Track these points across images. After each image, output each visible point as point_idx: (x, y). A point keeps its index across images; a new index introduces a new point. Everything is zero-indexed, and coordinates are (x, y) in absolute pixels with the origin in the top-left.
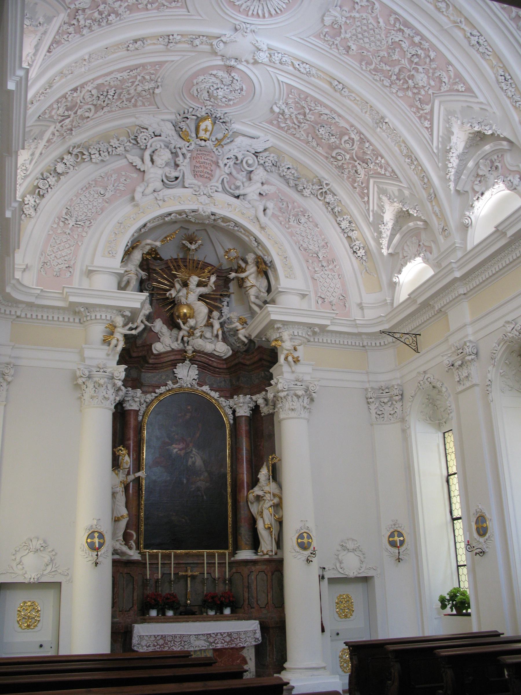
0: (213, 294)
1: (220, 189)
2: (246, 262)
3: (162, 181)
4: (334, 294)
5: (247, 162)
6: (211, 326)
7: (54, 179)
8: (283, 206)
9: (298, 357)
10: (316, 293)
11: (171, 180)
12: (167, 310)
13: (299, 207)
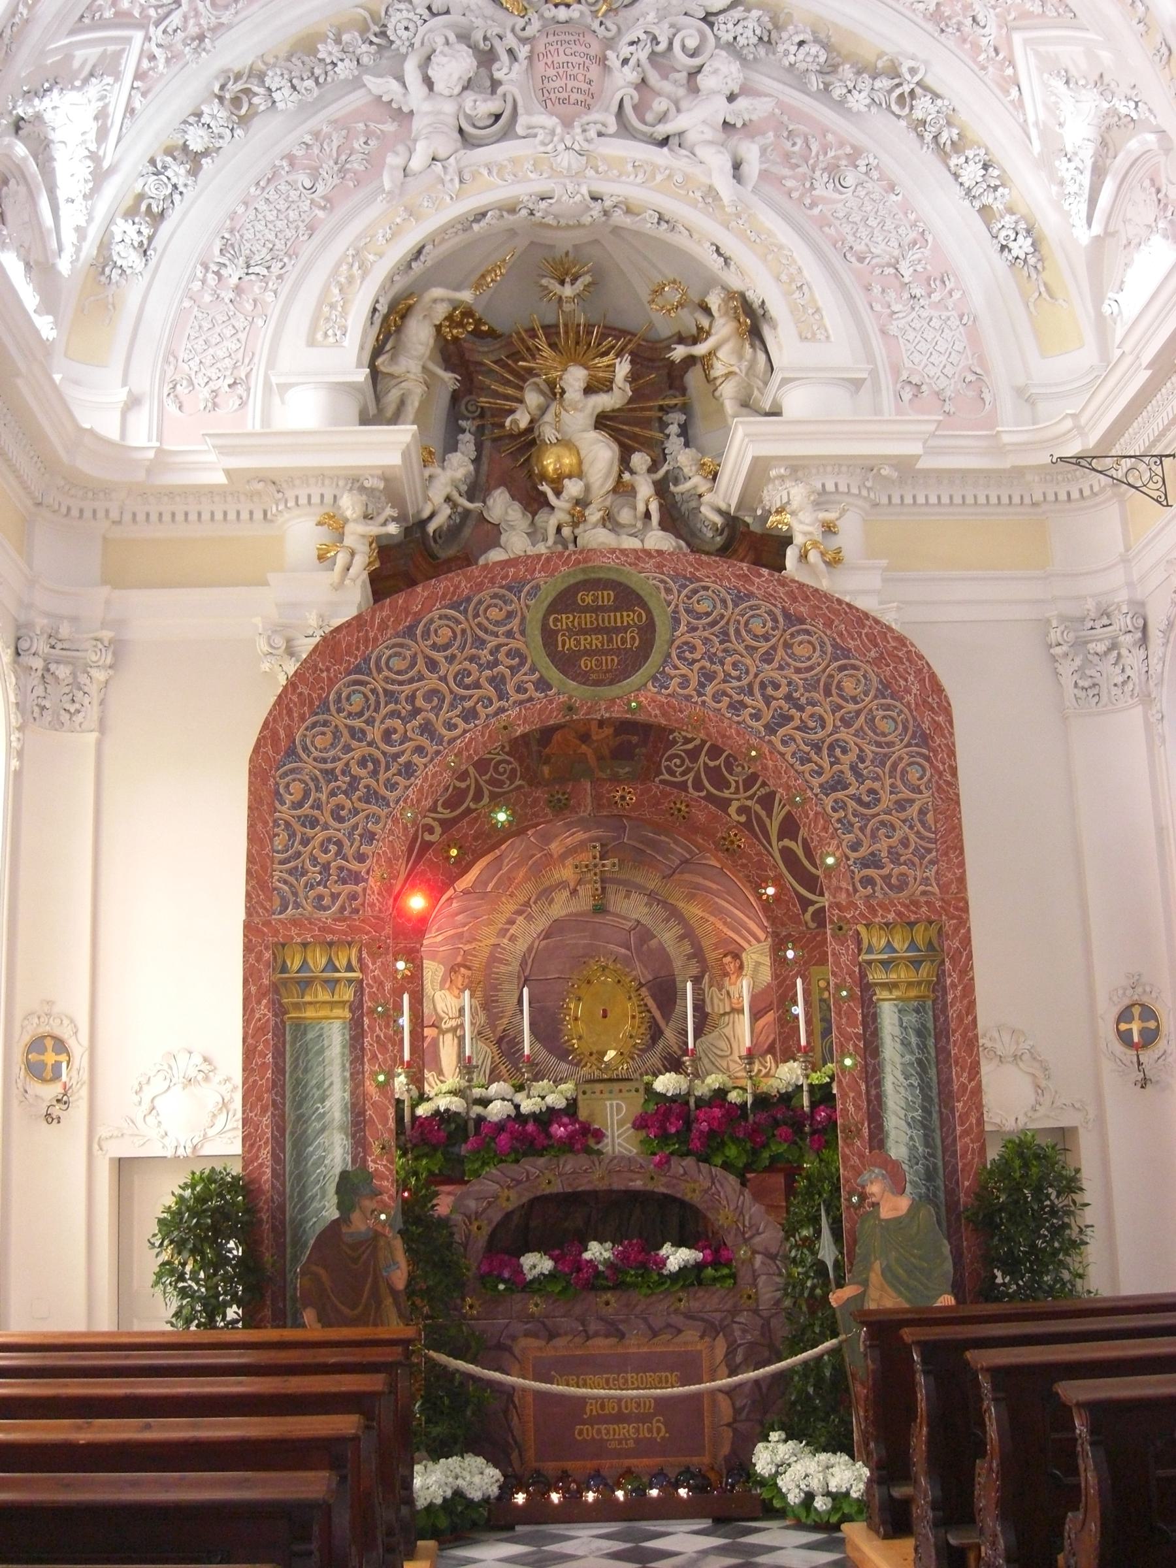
0: (631, 410)
1: (613, 127)
2: (707, 310)
3: (461, 131)
4: (949, 371)
5: (683, 47)
6: (632, 491)
7: (182, 170)
8: (796, 148)
9: (839, 551)
10: (896, 370)
11: (481, 124)
12: (514, 463)
13: (842, 145)
